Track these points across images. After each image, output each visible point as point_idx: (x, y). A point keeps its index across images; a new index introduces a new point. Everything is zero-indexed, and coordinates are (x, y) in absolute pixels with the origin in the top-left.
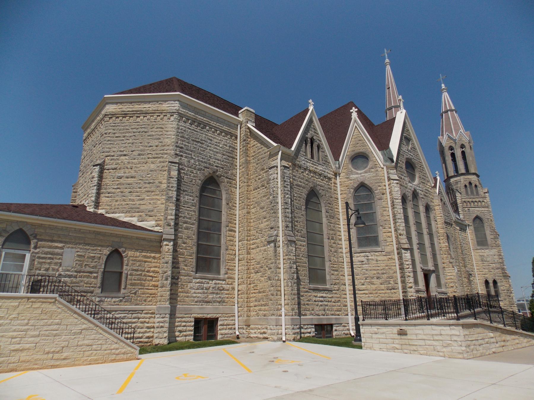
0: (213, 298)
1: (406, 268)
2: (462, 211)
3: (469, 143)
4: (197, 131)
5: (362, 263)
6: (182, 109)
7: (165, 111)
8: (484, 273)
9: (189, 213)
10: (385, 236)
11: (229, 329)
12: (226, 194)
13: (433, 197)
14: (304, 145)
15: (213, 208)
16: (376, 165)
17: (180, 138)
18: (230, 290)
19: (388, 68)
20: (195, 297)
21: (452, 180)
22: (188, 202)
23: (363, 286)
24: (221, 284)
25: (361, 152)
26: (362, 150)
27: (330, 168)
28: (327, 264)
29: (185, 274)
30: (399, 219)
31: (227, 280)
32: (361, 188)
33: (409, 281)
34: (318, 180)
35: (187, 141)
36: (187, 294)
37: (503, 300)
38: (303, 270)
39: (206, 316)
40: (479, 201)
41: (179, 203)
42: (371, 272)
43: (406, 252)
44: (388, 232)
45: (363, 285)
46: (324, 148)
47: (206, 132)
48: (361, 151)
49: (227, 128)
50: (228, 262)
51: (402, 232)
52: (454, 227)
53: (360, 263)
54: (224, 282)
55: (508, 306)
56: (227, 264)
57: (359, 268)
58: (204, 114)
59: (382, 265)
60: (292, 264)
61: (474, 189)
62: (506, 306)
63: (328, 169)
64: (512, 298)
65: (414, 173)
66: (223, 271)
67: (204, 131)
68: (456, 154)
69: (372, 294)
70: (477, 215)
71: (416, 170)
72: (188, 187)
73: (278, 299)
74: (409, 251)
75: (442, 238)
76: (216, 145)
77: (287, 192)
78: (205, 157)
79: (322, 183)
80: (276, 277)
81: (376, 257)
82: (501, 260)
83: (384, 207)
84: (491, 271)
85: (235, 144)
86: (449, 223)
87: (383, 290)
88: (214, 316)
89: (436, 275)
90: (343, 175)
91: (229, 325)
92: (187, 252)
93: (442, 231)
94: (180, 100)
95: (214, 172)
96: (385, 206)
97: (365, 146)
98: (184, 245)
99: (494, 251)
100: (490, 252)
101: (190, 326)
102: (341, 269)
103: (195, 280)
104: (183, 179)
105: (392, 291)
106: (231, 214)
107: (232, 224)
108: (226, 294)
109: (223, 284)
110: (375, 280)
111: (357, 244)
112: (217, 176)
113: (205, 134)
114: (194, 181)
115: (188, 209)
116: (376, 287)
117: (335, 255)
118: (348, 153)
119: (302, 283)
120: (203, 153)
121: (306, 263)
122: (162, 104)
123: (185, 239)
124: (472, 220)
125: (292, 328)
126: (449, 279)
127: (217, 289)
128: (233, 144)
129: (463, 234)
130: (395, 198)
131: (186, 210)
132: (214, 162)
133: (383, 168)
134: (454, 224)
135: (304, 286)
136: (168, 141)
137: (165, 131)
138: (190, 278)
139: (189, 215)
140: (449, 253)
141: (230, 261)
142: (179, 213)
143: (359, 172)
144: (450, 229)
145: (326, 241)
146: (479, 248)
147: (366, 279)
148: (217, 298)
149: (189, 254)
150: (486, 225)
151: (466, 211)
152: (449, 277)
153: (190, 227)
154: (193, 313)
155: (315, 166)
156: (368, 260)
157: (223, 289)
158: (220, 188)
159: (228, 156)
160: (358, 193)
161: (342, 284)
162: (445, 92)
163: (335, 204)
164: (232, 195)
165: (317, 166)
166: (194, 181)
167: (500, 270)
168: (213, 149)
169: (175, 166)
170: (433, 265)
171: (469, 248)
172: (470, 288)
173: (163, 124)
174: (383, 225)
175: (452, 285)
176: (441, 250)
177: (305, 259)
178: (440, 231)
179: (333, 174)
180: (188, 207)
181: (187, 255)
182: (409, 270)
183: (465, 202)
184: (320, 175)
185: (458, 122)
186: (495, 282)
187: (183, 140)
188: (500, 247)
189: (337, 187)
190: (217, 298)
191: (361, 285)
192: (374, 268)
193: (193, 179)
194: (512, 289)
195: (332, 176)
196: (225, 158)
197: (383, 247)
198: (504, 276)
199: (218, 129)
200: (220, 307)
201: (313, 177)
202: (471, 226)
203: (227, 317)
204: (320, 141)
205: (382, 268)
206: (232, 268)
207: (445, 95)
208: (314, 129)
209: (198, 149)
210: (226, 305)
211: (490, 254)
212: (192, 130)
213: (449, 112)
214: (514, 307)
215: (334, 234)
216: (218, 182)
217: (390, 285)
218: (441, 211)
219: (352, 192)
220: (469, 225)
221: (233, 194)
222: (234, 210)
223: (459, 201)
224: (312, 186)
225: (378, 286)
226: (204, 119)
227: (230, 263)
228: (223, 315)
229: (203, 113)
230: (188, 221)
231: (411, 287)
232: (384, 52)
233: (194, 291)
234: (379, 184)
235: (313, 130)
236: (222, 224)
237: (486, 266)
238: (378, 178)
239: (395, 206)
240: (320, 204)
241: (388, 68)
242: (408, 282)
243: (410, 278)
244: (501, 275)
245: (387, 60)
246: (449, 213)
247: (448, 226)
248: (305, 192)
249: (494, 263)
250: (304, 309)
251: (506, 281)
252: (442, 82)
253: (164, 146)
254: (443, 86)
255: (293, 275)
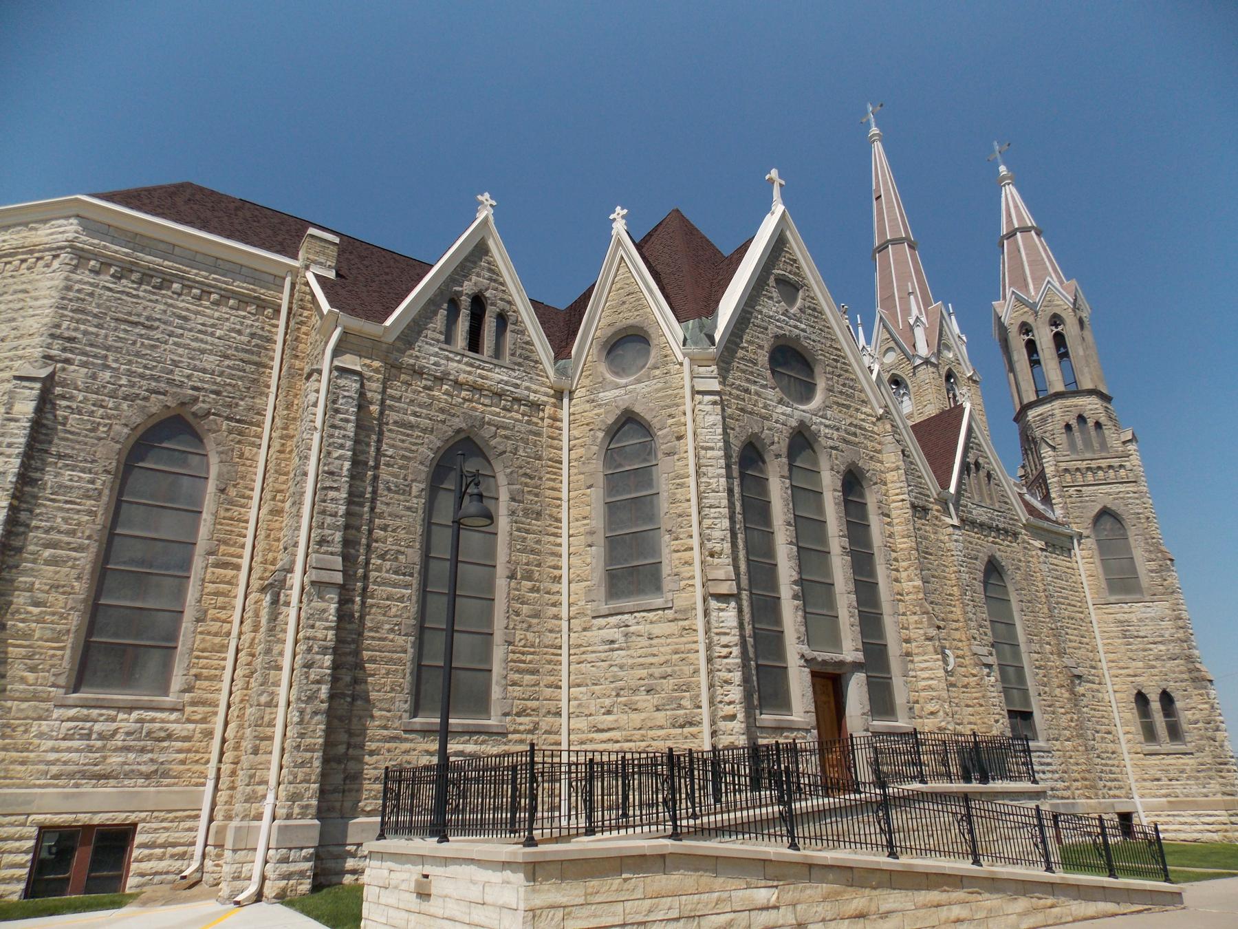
0: (125, 763)
1: (719, 657)
2: (1060, 496)
3: (1074, 311)
4: (137, 297)
5: (612, 646)
6: (86, 238)
7: (41, 247)
8: (1132, 673)
9: (70, 518)
10: (677, 562)
11: (172, 856)
12: (221, 462)
13: (879, 447)
14: (442, 313)
15: (172, 500)
16: (666, 356)
17: (71, 314)
18: (195, 739)
19: (878, 148)
20: (53, 763)
21: (1032, 414)
22: (72, 488)
23: (610, 718)
24: (163, 721)
25: (632, 327)
26: (629, 318)
27: (542, 376)
28: (499, 652)
29: (22, 695)
30: (710, 507)
31: (188, 709)
32: (626, 427)
33: (726, 699)
34: (489, 409)
35: (96, 321)
36: (25, 754)
37: (1193, 751)
38: (388, 674)
39: (84, 819)
40: (1110, 467)
41: (36, 490)
42: (632, 672)
43: (724, 606)
44: (685, 550)
45: (609, 712)
46: (522, 322)
47: (171, 298)
48: (630, 322)
49: (245, 285)
50: (198, 657)
51: (718, 547)
52: (1024, 542)
53: (607, 647)
54: (174, 716)
55: (1210, 769)
56: (195, 661)
57: (603, 661)
58: (168, 249)
59: (664, 650)
60: (317, 653)
61: (1093, 433)
62: (1203, 770)
63: (531, 378)
64: (1222, 746)
65: (813, 378)
66: (177, 683)
67: (164, 296)
68: (1038, 343)
69: (631, 741)
70: (1105, 507)
71: (818, 370)
72: (77, 447)
73: (261, 764)
74: (733, 604)
75: (905, 564)
76: (200, 332)
77: (340, 441)
78: (155, 364)
79: (504, 417)
80: (261, 694)
81: (648, 626)
82: (1181, 631)
83: (678, 477)
84: (1154, 667)
85: (274, 330)
86: (1006, 532)
87: (661, 727)
88: (120, 818)
89: (868, 677)
90: (580, 395)
91: (174, 845)
92: (42, 628)
93: (904, 543)
94: (82, 213)
95: (183, 404)
96: (682, 472)
97: (644, 307)
98: (36, 610)
99: (1160, 608)
100: (1149, 610)
101: (18, 851)
102: (550, 667)
103: (62, 711)
104: (64, 425)
105: (687, 730)
106: (232, 519)
107: (232, 546)
108: (180, 751)
109: (168, 722)
110: (641, 699)
111: (603, 589)
112: (194, 414)
113: (165, 304)
114: (105, 429)
115: (68, 506)
116: (643, 720)
117: (530, 626)
118: (599, 333)
119: (376, 713)
120: (149, 352)
121: (405, 652)
122: (36, 229)
123: (43, 591)
124: (1090, 521)
125: (278, 857)
126: (923, 690)
127: (146, 736)
128: (267, 328)
129: (1059, 560)
130: (705, 444)
131: (61, 509)
132: (189, 377)
133: (681, 364)
134: (1023, 531)
135: (383, 723)
136: (33, 324)
137: (31, 298)
138: (42, 705)
139: (70, 524)
140: (923, 610)
141: (205, 654)
142: (31, 519)
143: (623, 381)
144: (1008, 546)
145: (501, 583)
146: (1113, 599)
147: (618, 695)
148: (139, 764)
149: (48, 634)
150: (1132, 532)
151: (1070, 497)
152: (924, 683)
153: (68, 557)
154: (34, 810)
155: (479, 371)
156: (626, 635)
157: (169, 737)
158: (204, 448)
159: (242, 360)
160: (618, 442)
161: (549, 712)
162: (1009, 184)
163: (548, 476)
164: (243, 465)
165: (490, 370)
166: (105, 429)
167: (1182, 662)
168: (189, 342)
169: (32, 389)
170: (860, 647)
171: (1083, 601)
172: (1075, 717)
173: (30, 282)
174: (674, 529)
175: (932, 709)
176: (900, 600)
177: (400, 640)
178: (900, 543)
179: (552, 392)
180: (67, 502)
181: (41, 639)
182: (727, 664)
183: (1066, 470)
184: (499, 395)
185: (1043, 259)
186: (1167, 699)
187: (80, 319)
188: (1176, 596)
189: (560, 429)
190: (139, 764)
191: (604, 714)
192: (642, 660)
193: (99, 424)
194: (1221, 718)
195: (545, 399)
196: (228, 367)
197: (670, 595)
198: (1194, 680)
199: (212, 290)
200: (149, 792)
201: (470, 401)
202: (1088, 537)
203: (172, 821)
204: (509, 303)
205: (662, 659)
206: (213, 672)
207: (1010, 194)
208: (490, 270)
209: (134, 343)
210: (174, 784)
211: (1148, 615)
212: (118, 292)
213: (1018, 234)
214: (1229, 771)
215: (535, 563)
216: (199, 432)
217: (682, 712)
218: (902, 485)
219: (599, 440)
220: (1080, 536)
221: (248, 462)
222: (242, 506)
223: (1049, 470)
224: (463, 425)
225: (649, 714)
226: (166, 263)
227: (206, 658)
228: (155, 814)
229: (162, 246)
230: (61, 541)
231: (733, 717)
232: (866, 113)
233: (50, 743)
234: (669, 411)
235: (487, 274)
236: (198, 547)
237: (1136, 650)
238: (670, 392)
239: (704, 469)
240: (494, 477)
241: (878, 148)
242: (721, 702)
243: (729, 687)
244: (1185, 676)
245: (874, 130)
246: (1006, 503)
247: (1002, 537)
248: (431, 442)
249: (1160, 642)
250: (373, 793)
251: (1201, 695)
252: (1000, 160)
253: (22, 336)
254: (1003, 169)
255: (315, 687)
